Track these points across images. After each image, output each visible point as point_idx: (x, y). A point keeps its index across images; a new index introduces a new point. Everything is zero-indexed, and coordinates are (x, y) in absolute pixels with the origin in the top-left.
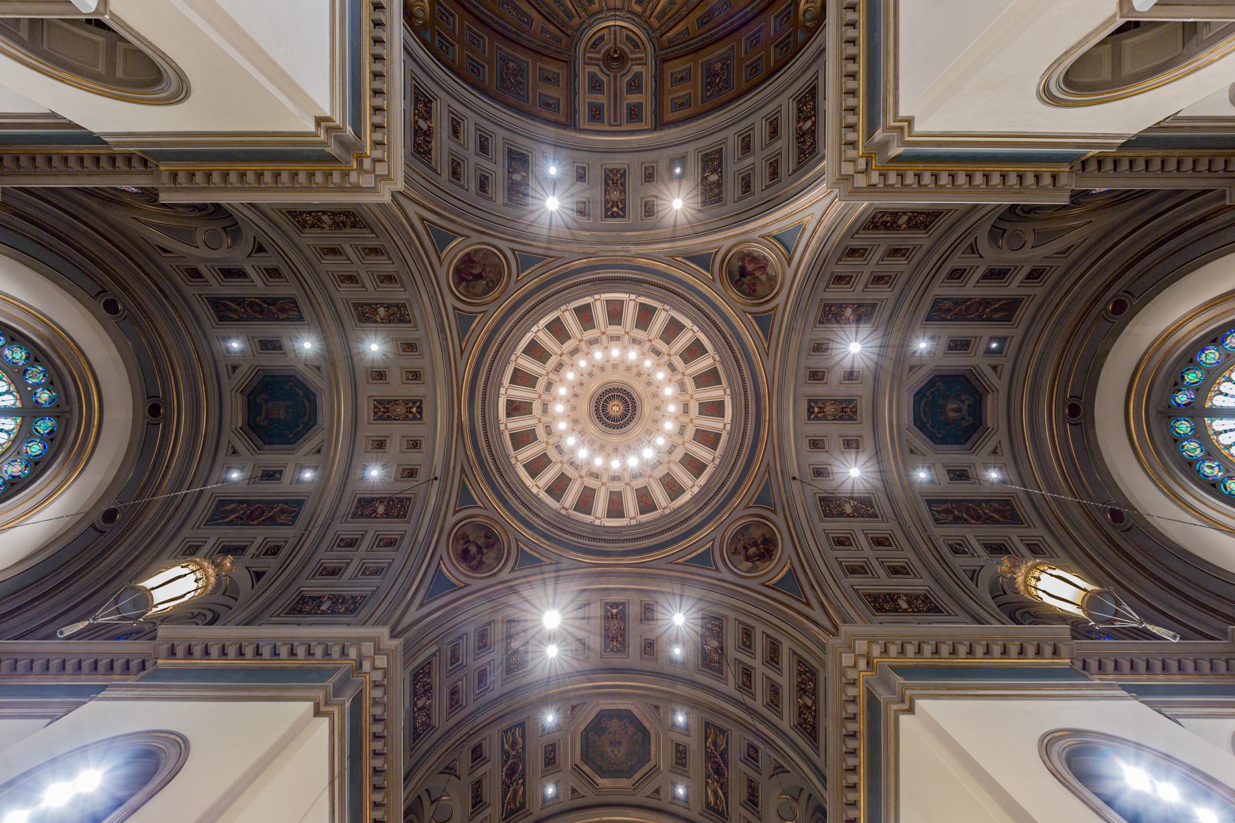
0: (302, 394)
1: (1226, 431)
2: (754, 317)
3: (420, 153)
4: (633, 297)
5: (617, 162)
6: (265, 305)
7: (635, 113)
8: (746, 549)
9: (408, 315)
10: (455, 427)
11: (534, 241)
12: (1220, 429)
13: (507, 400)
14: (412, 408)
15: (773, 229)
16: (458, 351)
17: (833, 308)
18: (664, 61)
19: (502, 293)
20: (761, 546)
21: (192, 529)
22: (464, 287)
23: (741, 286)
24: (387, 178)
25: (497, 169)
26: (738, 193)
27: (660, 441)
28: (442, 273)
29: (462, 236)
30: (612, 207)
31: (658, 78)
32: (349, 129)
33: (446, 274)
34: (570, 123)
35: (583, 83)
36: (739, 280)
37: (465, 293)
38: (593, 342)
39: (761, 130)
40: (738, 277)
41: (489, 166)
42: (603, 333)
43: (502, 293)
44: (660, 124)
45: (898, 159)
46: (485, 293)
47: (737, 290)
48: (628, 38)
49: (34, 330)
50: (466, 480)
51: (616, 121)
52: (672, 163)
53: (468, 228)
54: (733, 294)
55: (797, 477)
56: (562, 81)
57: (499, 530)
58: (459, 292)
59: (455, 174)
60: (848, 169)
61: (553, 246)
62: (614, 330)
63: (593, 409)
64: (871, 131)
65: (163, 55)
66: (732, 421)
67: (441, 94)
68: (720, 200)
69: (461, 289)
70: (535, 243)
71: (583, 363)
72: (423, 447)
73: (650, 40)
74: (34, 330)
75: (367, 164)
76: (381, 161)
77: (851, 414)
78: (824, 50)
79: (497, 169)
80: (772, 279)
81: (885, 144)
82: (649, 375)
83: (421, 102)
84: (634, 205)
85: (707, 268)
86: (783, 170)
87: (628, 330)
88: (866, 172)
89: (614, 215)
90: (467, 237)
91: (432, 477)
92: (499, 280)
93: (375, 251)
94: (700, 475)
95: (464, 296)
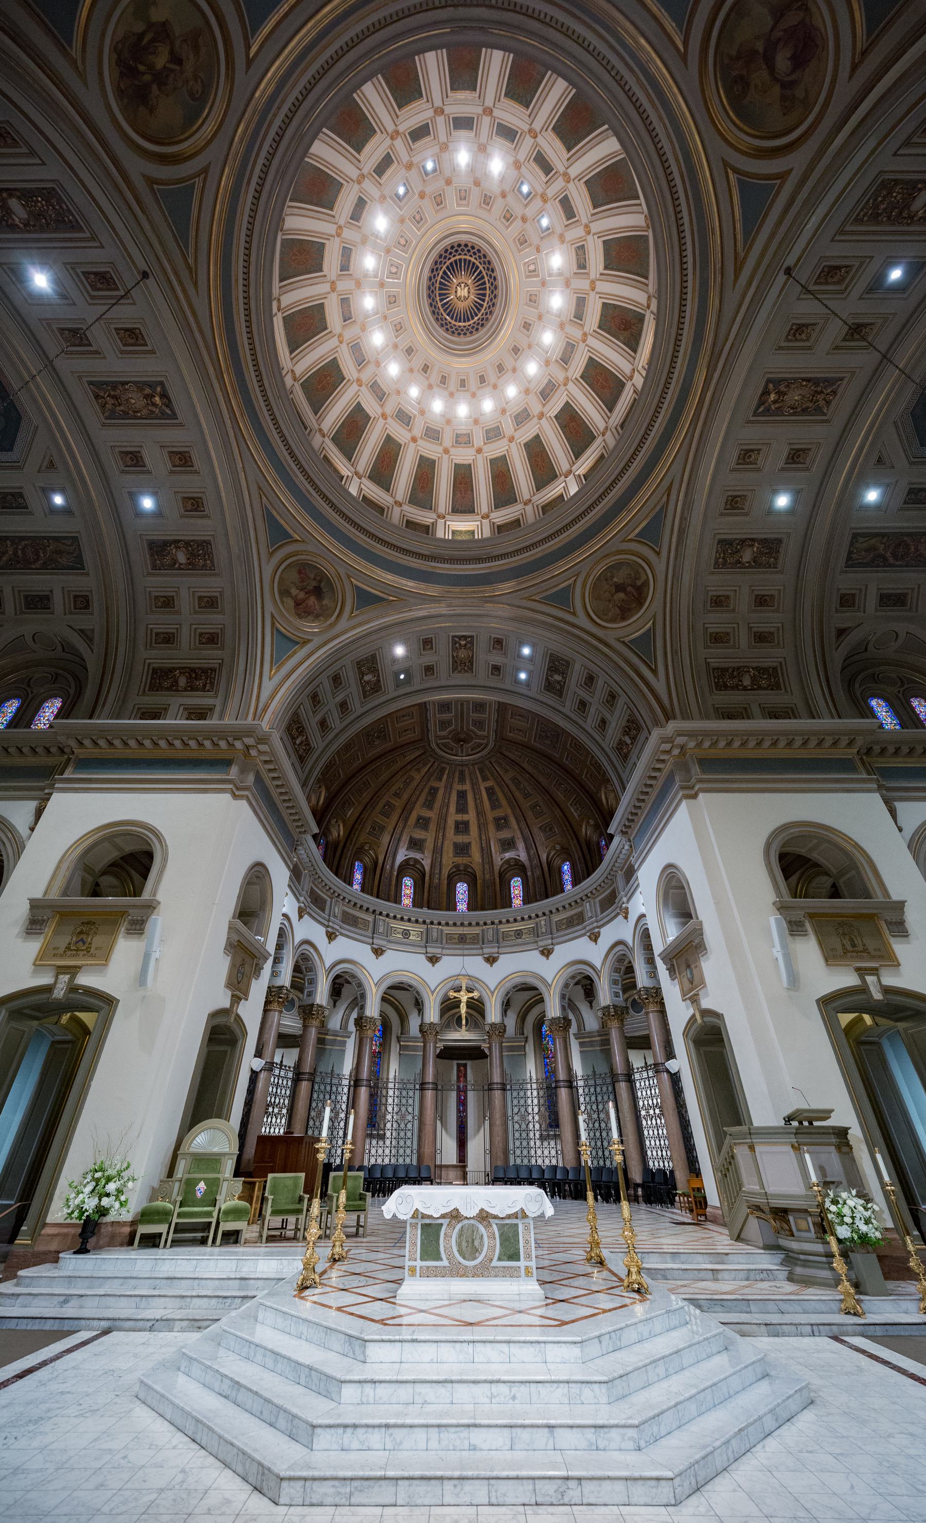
5: (459, 679)
8: (176, 59)
14: (775, 402)
16: (673, 497)
18: (421, 740)
20: (147, 77)
22: (639, 579)
31: (425, 729)
33: (654, 602)
34: (502, 708)
36: (320, 581)
37: (641, 570)
40: (322, 584)
46: (618, 566)
47: (318, 568)
50: (740, 244)
51: (462, 705)
58: (647, 576)
59: (612, 697)
60: (262, 747)
63: (498, 273)
69: (644, 577)
70: (550, 620)
71: (512, 391)
73: (433, 750)
78: (302, 787)
81: (243, 771)
83: (624, 752)
88: (248, 748)
92: (599, 579)
95: (640, 565)
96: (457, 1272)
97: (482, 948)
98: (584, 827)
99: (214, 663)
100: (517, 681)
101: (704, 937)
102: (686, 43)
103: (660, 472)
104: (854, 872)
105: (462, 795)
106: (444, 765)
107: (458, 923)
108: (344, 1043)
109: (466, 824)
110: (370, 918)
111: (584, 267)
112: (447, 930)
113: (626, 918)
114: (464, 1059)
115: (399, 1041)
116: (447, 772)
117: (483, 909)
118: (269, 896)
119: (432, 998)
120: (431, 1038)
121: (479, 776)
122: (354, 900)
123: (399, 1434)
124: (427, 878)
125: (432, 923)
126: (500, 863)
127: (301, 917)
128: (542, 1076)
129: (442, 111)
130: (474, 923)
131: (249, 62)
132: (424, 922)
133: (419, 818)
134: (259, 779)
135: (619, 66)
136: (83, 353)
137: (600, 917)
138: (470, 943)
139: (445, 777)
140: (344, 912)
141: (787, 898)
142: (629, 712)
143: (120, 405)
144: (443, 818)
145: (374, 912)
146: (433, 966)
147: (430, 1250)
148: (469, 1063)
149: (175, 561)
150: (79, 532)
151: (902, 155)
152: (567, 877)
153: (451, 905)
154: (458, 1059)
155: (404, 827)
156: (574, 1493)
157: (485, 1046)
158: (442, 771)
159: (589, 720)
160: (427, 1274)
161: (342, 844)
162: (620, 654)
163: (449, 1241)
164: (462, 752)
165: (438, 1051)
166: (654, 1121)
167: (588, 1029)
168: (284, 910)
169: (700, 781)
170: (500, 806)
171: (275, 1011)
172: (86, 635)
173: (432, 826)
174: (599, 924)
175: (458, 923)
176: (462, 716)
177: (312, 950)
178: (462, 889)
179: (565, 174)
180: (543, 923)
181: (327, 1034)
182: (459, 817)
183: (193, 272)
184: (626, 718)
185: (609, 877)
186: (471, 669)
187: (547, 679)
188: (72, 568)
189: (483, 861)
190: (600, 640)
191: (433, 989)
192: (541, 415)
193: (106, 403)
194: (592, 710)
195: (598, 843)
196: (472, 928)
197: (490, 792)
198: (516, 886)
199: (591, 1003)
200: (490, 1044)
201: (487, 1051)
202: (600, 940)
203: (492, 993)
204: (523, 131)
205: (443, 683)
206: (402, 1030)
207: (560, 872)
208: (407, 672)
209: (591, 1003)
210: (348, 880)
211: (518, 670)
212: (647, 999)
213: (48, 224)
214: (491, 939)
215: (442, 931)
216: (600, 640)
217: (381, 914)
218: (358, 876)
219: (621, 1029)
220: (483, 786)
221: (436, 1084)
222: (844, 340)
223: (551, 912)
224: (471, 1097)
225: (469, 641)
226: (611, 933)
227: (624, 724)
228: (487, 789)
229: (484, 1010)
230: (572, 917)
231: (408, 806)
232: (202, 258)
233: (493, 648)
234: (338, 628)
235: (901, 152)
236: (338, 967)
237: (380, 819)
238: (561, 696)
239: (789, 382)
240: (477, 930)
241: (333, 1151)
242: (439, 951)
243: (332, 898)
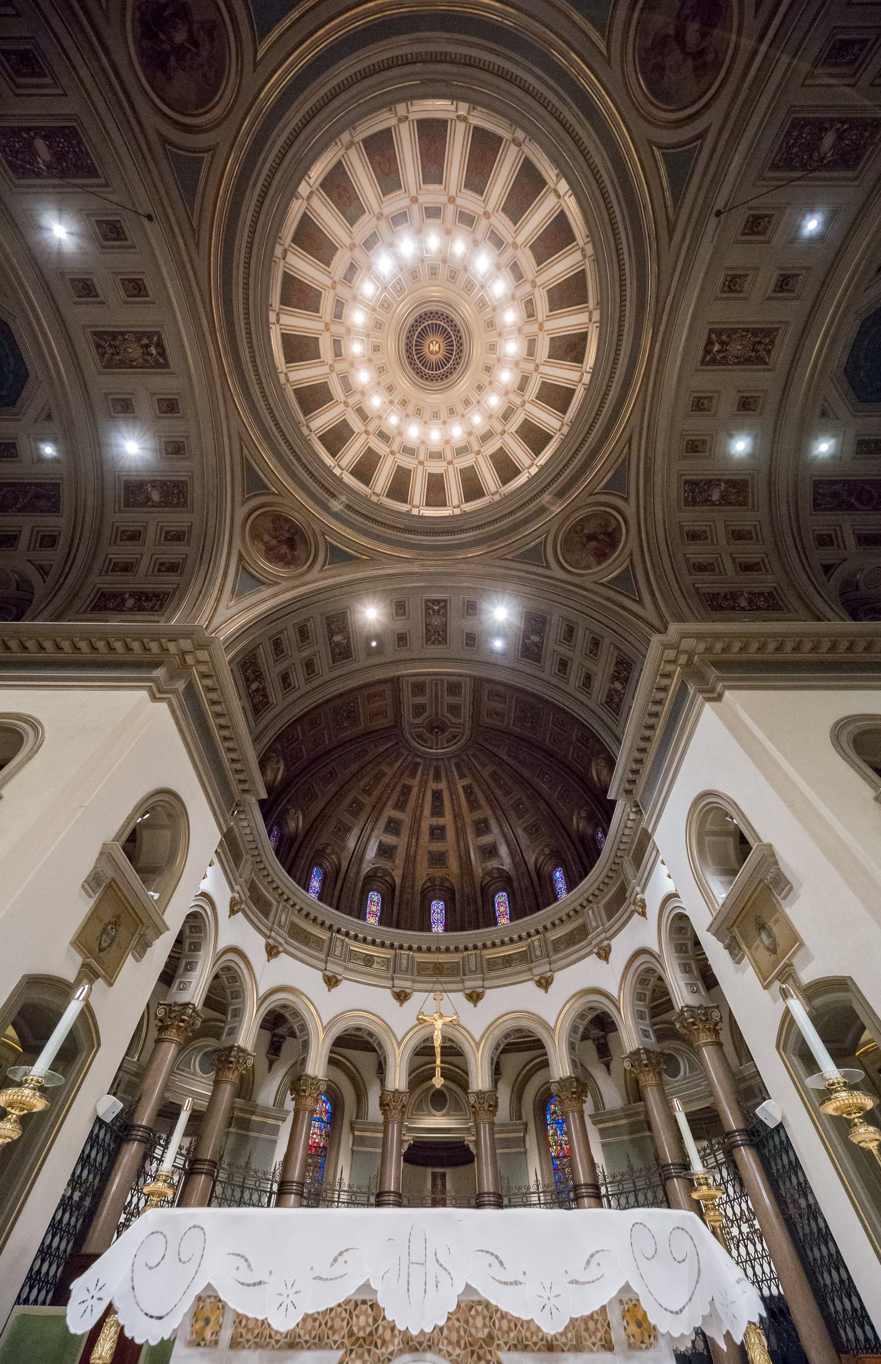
0: (862, 374)
2: (268, 489)
3: (627, 663)
4: (415, 512)
5: (433, 651)
6: (853, 500)
7: (419, 688)
8: (192, 39)
9: (685, 491)
10: (665, 318)
11: (524, 578)
13: (582, 362)
14: (719, 351)
15: (266, 592)
16: (635, 445)
17: (175, 501)
19: (568, 517)
20: (167, 47)
23: (290, 528)
24: (666, 647)
25: (553, 645)
26: (310, 625)
27: (368, 289)
28: (633, 544)
29: (602, 584)
30: (439, 610)
31: (398, 715)
32: (691, 690)
33: (628, 543)
34: (478, 683)
35: (466, 711)
36: (293, 534)
38: (462, 451)
39: (298, 678)
41: (562, 649)
42: (450, 463)
43: (568, 517)
44: (395, 682)
45: (156, 665)
48: (426, 741)
50: (670, 210)
51: (436, 684)
52: (379, 650)
53: (596, 593)
54: (298, 518)
55: (145, 221)
56: (484, 713)
57: (635, 87)
59: (596, 643)
60: (202, 655)
61: (504, 571)
62: (436, 468)
63: (465, 347)
64: (190, 690)
65: (846, 757)
66: (269, 329)
67: (597, 709)
68: (328, 618)
69: (614, 523)
70: (523, 574)
71: (477, 419)
72: (721, 278)
73: (407, 740)
75: (683, 659)
76: (669, 662)
77: (103, 343)
79: (553, 645)
80: (256, 536)
81: (173, 676)
82: (391, 402)
84: (417, 612)
85: (333, 548)
86: (269, 646)
87: (420, 467)
88: (183, 653)
89: (437, 602)
90: (596, 583)
91: (723, 216)
93: (701, 568)
94: (437, 121)
95: (610, 513)
97: (463, 981)
98: (575, 820)
99: (169, 587)
101: (782, 866)
102: (608, 49)
103: (619, 428)
105: (437, 796)
106: (418, 760)
108: (275, 1130)
109: (443, 828)
110: (324, 935)
111: (533, 316)
112: (420, 957)
113: (643, 914)
114: (443, 1166)
115: (352, 1129)
118: (182, 842)
120: (395, 1114)
122: (306, 909)
124: (397, 893)
125: (401, 947)
127: (233, 912)
129: (417, 200)
131: (256, 65)
132: (392, 946)
133: (390, 821)
134: (190, 690)
135: (555, 101)
137: (608, 924)
138: (448, 975)
139: (419, 773)
140: (293, 924)
143: (118, 354)
144: (417, 820)
145: (331, 927)
146: (401, 1005)
148: (448, 1171)
149: (148, 499)
150: (61, 479)
151: (810, 86)
152: (561, 885)
154: (434, 1165)
155: (372, 830)
157: (469, 1139)
158: (416, 766)
161: (299, 839)
162: (601, 596)
165: (406, 1147)
166: (742, 1250)
167: (608, 1107)
168: (205, 886)
170: (479, 807)
171: (171, 1041)
172: (43, 571)
176: (437, 697)
177: (242, 965)
179: (514, 243)
180: (536, 943)
181: (253, 1113)
182: (435, 821)
183: (196, 233)
186: (445, 639)
188: (49, 511)
189: (461, 872)
190: (576, 586)
191: (399, 1039)
192: (503, 432)
193: (105, 353)
194: (575, 666)
195: (594, 838)
196: (450, 955)
198: (501, 900)
199: (607, 1066)
200: (478, 1135)
201: (472, 1148)
202: (612, 957)
203: (478, 1045)
204: (479, 216)
205: (414, 655)
206: (358, 1112)
207: (552, 880)
209: (607, 1066)
210: (303, 881)
212: (694, 1024)
213: (69, 169)
214: (473, 968)
216: (576, 586)
217: (339, 931)
218: (315, 884)
220: (460, 784)
222: (775, 291)
223: (545, 928)
225: (443, 604)
229: (467, 1082)
230: (572, 932)
232: (206, 227)
234: (309, 577)
235: (808, 82)
236: (275, 997)
237: (347, 818)
238: (539, 661)
239: (731, 332)
240: (456, 958)
242: (408, 984)
243: (279, 902)
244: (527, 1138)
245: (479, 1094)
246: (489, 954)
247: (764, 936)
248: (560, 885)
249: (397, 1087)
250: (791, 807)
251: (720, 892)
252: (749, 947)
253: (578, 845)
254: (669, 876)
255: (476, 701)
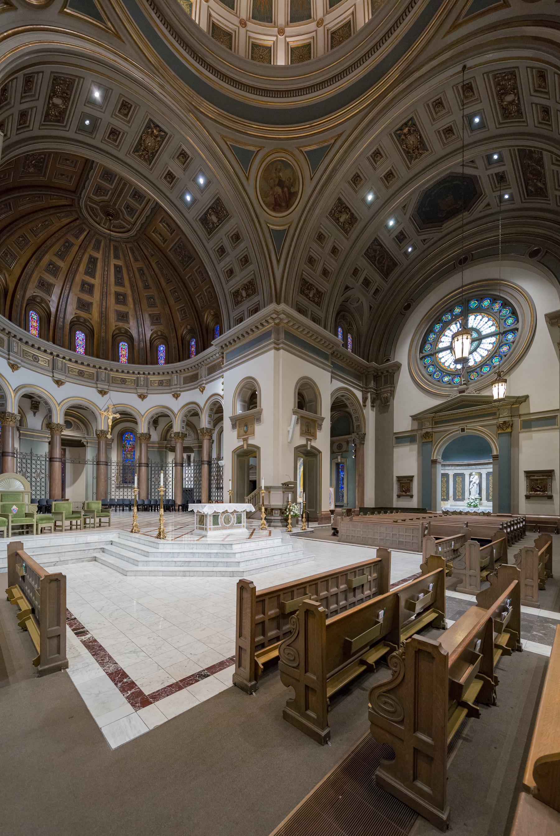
1: (481, 320)
12: (484, 319)
21: (550, 204)
24: (276, 312)
37: (297, 183)
49: (425, 328)
73: (80, 209)
74: (425, 328)
96: (224, 528)
98: (183, 328)
100: (182, 198)
104: (314, 403)
106: (84, 226)
107: (79, 362)
109: (92, 287)
116: (85, 233)
117: (98, 357)
119: (58, 408)
121: (112, 252)
123: (259, 560)
124: (52, 319)
126: (114, 328)
128: (121, 460)
130: (91, 365)
136: (431, 112)
139: (82, 237)
141: (296, 408)
142: (252, 277)
147: (216, 522)
153: (116, 358)
156: (299, 562)
158: (82, 231)
159: (222, 264)
160: (215, 529)
163: (221, 520)
164: (105, 224)
169: (283, 343)
173: (62, 276)
174: (181, 390)
175: (79, 362)
178: (80, 337)
180: (142, 379)
184: (249, 279)
185: (196, 366)
187: (206, 214)
194: (228, 259)
197: (118, 269)
199: (156, 428)
205: (121, 155)
207: (157, 350)
208: (95, 121)
209: (156, 428)
211: (187, 190)
214: (103, 379)
215: (109, 375)
219: (182, 443)
221: (148, 464)
223: (149, 374)
224: (68, 466)
226: (187, 397)
227: (245, 282)
228: (116, 267)
231: (43, 248)
233: (178, 157)
241: (167, 490)
244: (113, 444)
245: (142, 434)
246: (113, 374)
247: (245, 428)
248: (161, 355)
249: (59, 422)
250: (274, 404)
251: (239, 411)
252: (239, 427)
253: (180, 342)
254: (223, 390)
255: (150, 219)
